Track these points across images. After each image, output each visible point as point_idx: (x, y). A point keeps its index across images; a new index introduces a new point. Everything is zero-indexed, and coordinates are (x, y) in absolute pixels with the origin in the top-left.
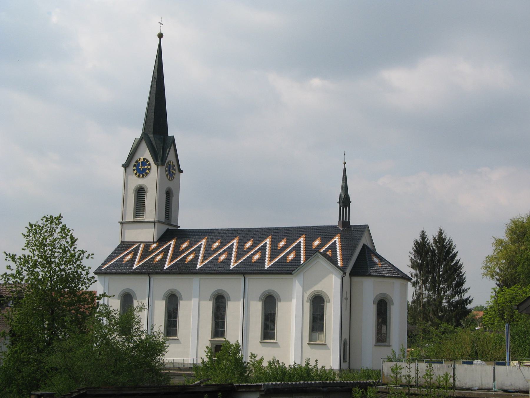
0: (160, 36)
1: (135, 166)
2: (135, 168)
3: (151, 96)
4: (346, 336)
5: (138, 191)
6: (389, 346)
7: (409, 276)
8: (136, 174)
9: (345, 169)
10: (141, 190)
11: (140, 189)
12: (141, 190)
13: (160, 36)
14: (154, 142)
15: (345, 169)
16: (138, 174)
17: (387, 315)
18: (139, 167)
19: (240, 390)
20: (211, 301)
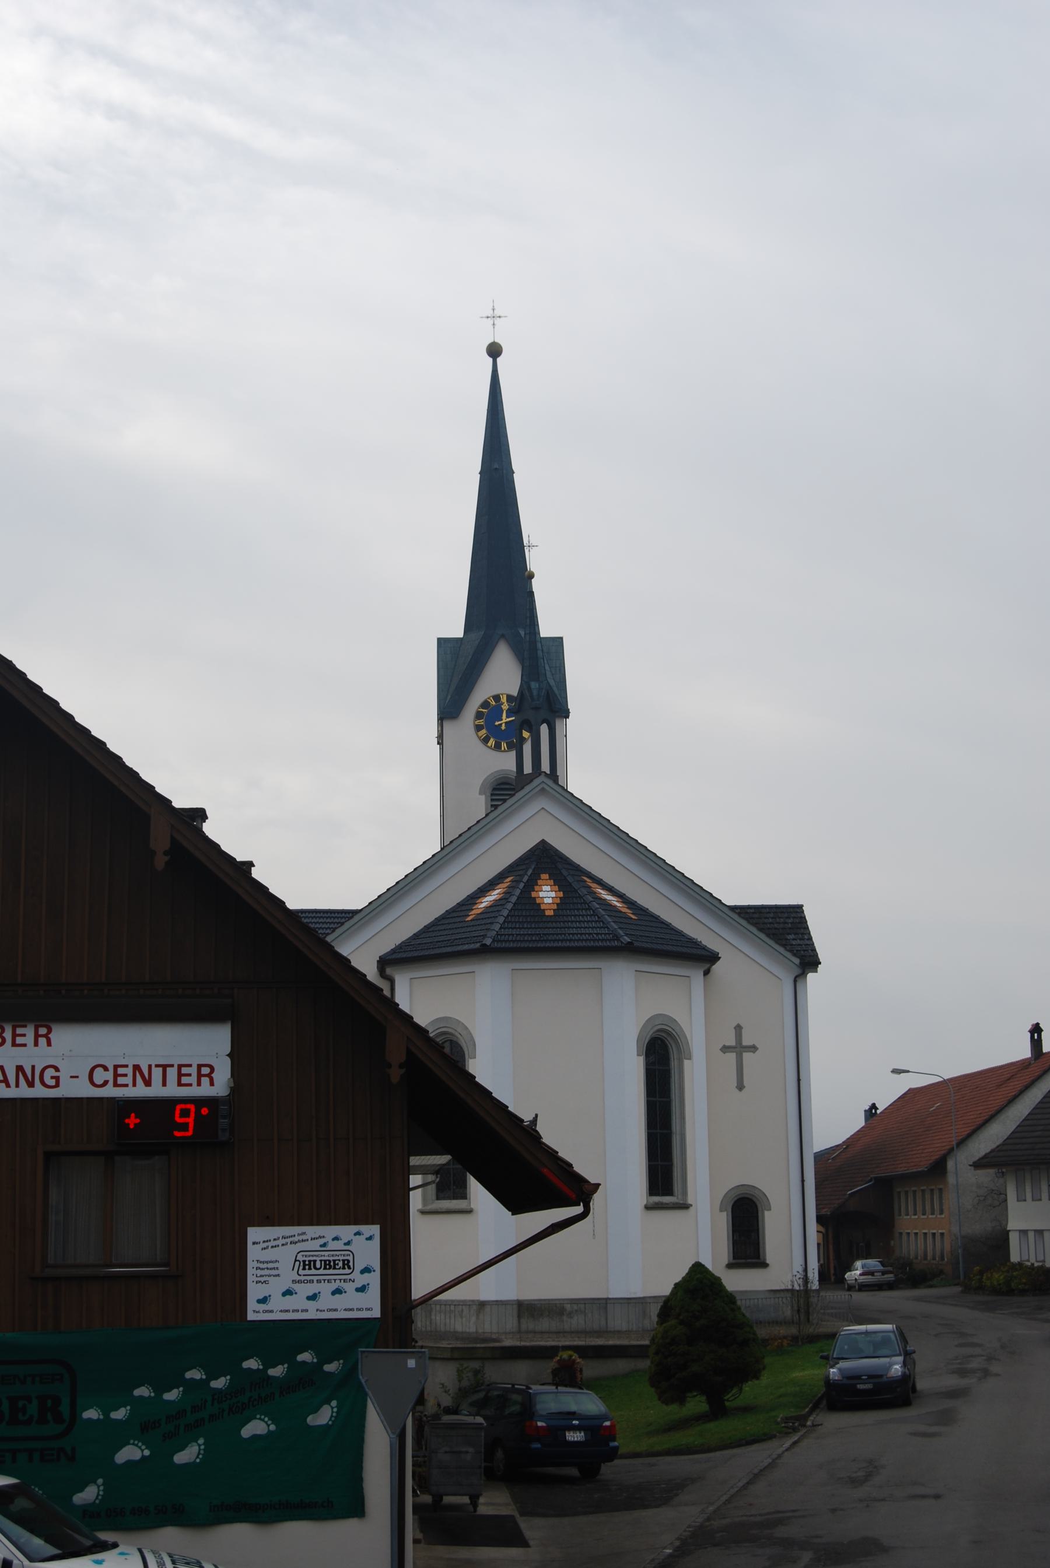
0: (494, 351)
1: (479, 715)
2: (481, 722)
3: (561, 654)
4: (876, 1288)
5: (494, 789)
6: (685, 1207)
7: (440, 1295)
8: (485, 741)
9: (908, 1071)
10: (502, 787)
11: (499, 785)
12: (502, 787)
13: (494, 351)
14: (863, 1385)
15: (908, 1071)
16: (492, 740)
17: (61, 1096)
18: (503, 727)
19: (845, 1328)
20: (482, 795)
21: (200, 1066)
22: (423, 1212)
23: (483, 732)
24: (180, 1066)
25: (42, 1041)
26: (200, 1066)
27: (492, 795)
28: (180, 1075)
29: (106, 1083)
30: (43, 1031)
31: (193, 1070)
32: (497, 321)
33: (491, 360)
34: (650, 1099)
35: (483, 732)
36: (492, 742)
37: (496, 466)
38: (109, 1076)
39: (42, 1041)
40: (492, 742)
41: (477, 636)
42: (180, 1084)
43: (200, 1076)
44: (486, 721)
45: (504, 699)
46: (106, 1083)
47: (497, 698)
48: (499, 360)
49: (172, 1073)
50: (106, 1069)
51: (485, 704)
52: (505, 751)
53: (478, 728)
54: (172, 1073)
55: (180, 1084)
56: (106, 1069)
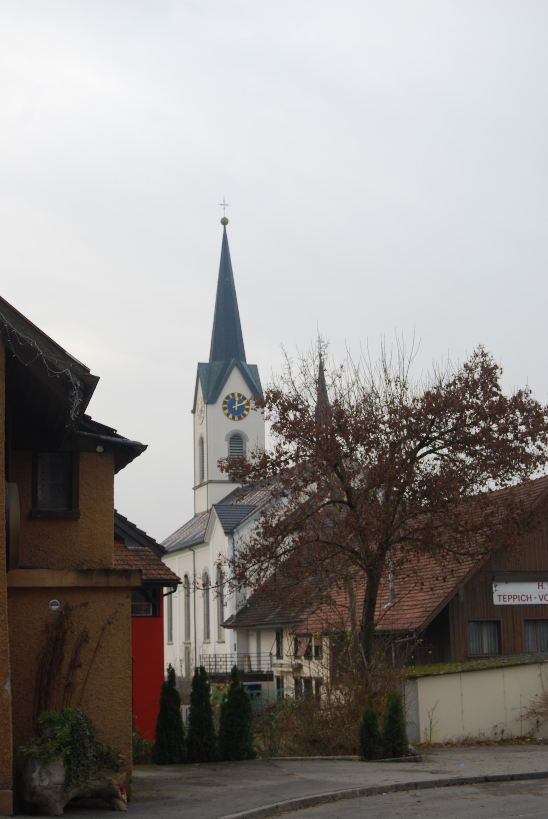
0: (225, 222)
1: (225, 403)
2: (226, 406)
5: (231, 439)
8: (228, 415)
11: (233, 436)
13: (225, 222)
21: (509, 596)
22: (168, 644)
23: (227, 411)
24: (504, 596)
25: (541, 587)
26: (509, 596)
27: (230, 441)
28: (504, 598)
29: (525, 600)
30: (540, 584)
31: (507, 597)
32: (226, 207)
33: (222, 226)
34: (133, 603)
35: (227, 411)
36: (231, 416)
37: (227, 279)
38: (526, 598)
39: (541, 587)
40: (231, 416)
41: (219, 364)
42: (504, 601)
43: (509, 599)
44: (228, 406)
45: (236, 395)
46: (525, 600)
47: (233, 395)
48: (227, 226)
49: (502, 598)
50: (525, 596)
51: (228, 397)
52: (237, 420)
53: (224, 409)
54: (502, 598)
55: (504, 601)
56: (525, 596)
